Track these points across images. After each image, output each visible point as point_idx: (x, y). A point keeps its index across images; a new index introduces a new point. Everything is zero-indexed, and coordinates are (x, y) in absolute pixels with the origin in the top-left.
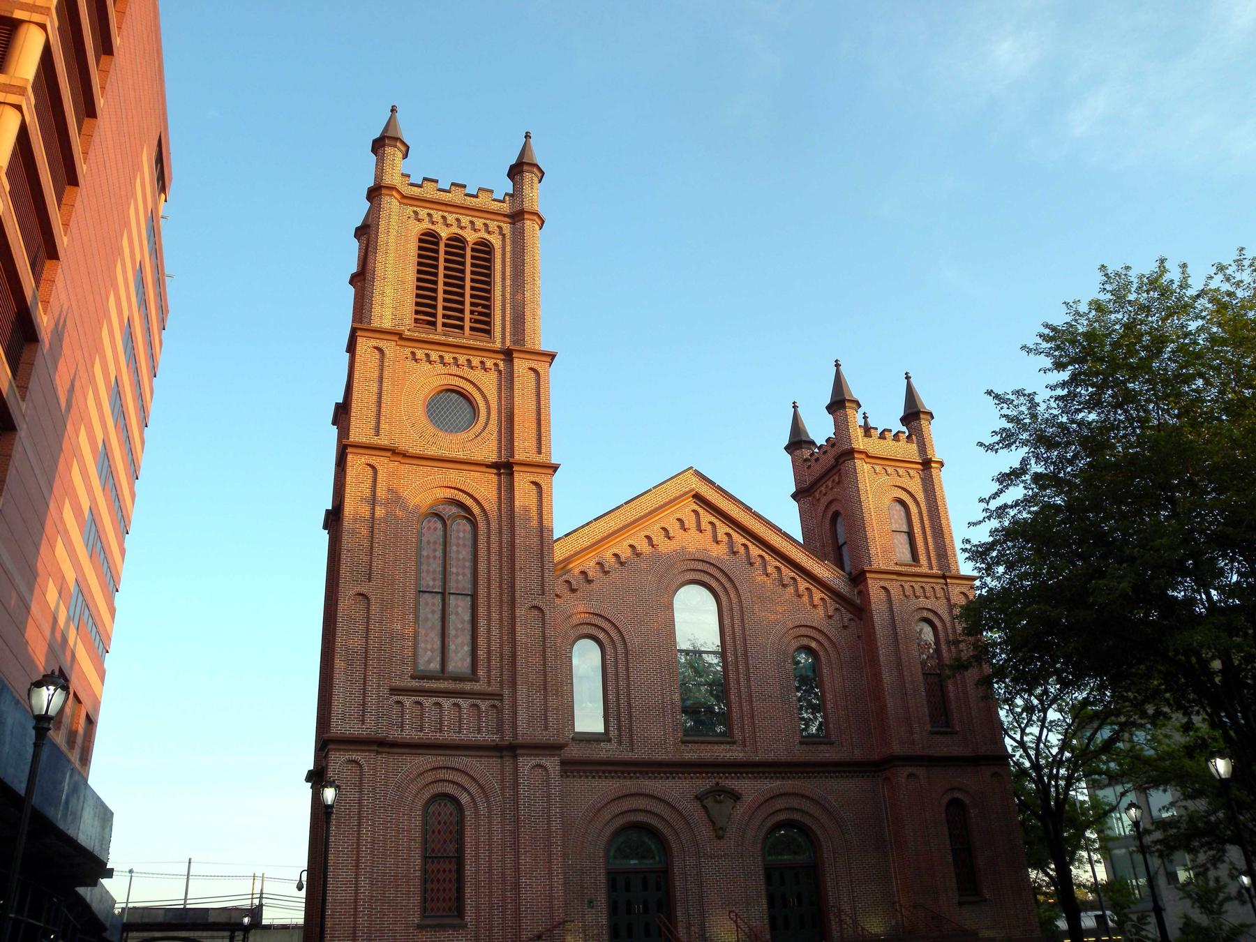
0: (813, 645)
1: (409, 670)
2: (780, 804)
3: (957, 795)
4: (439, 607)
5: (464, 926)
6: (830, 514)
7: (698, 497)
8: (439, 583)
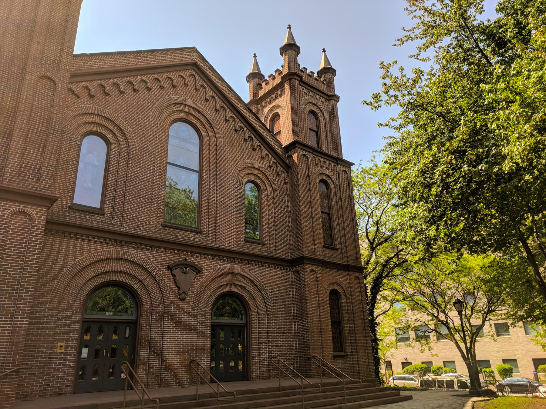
0: (258, 181)
3: (337, 288)
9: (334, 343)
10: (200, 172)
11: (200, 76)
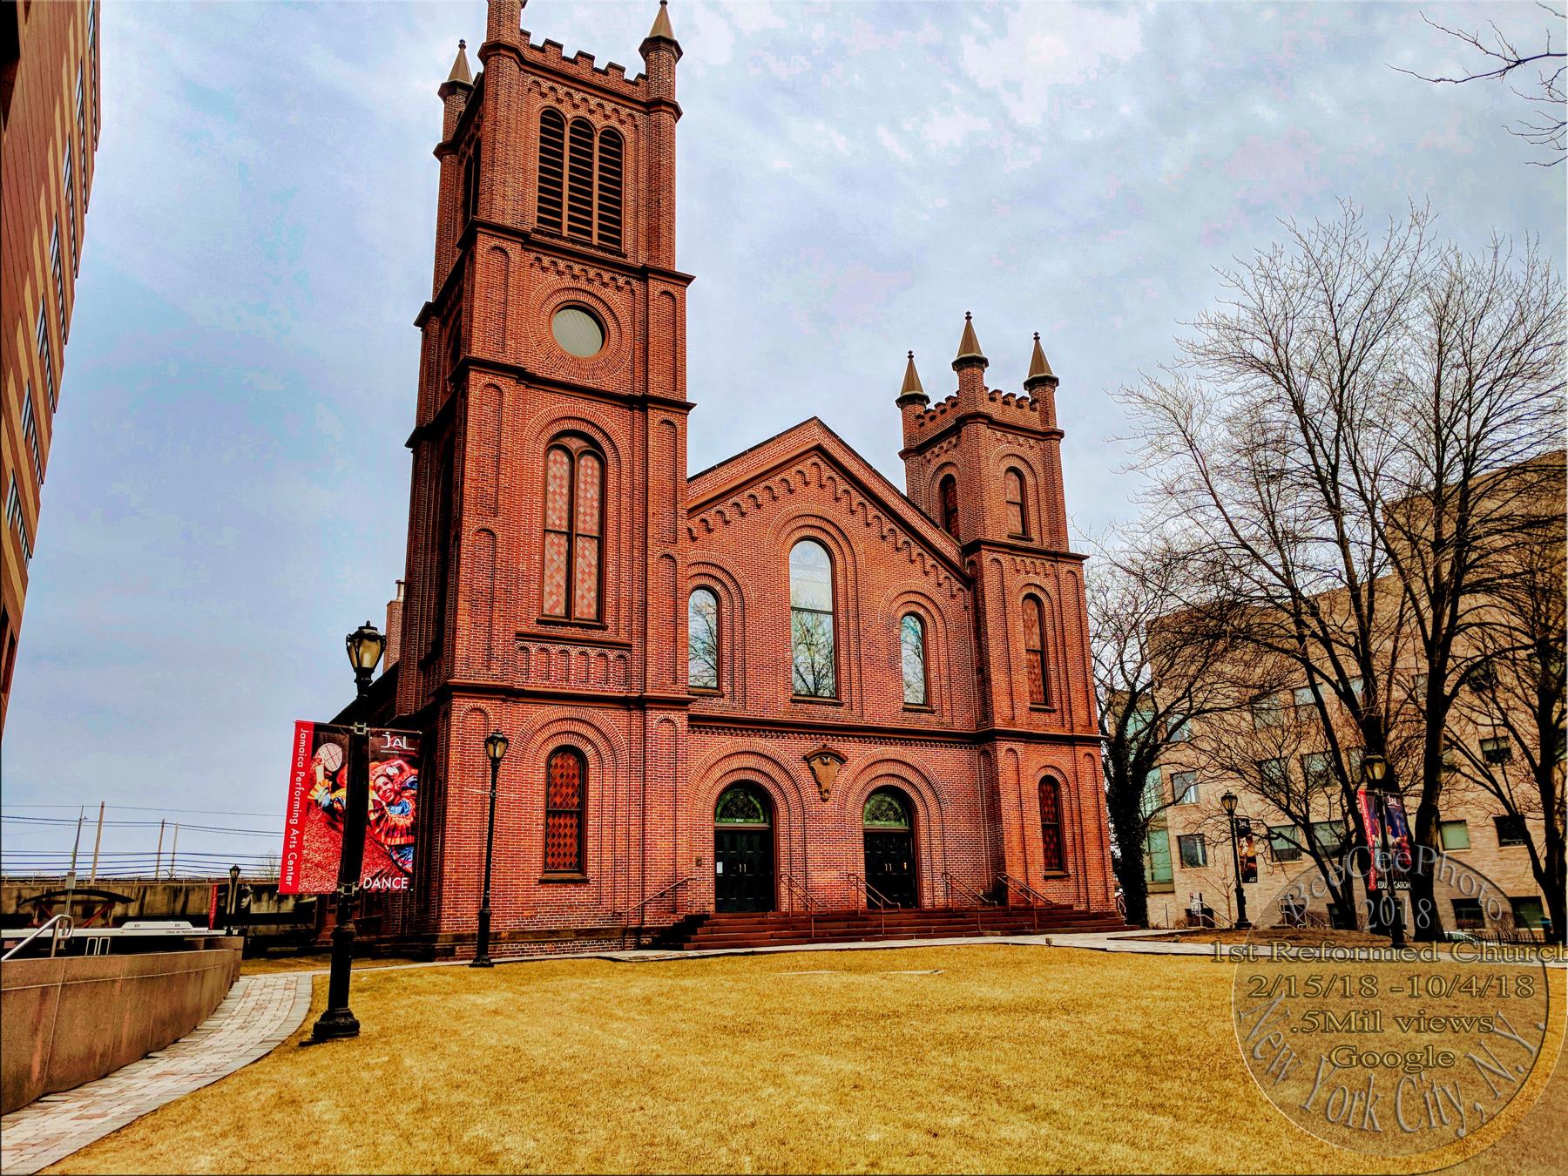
0: (921, 612)
1: (535, 616)
2: (736, 763)
4: (564, 549)
5: (586, 882)
7: (819, 449)
8: (565, 523)
9: (1046, 857)
10: (834, 613)
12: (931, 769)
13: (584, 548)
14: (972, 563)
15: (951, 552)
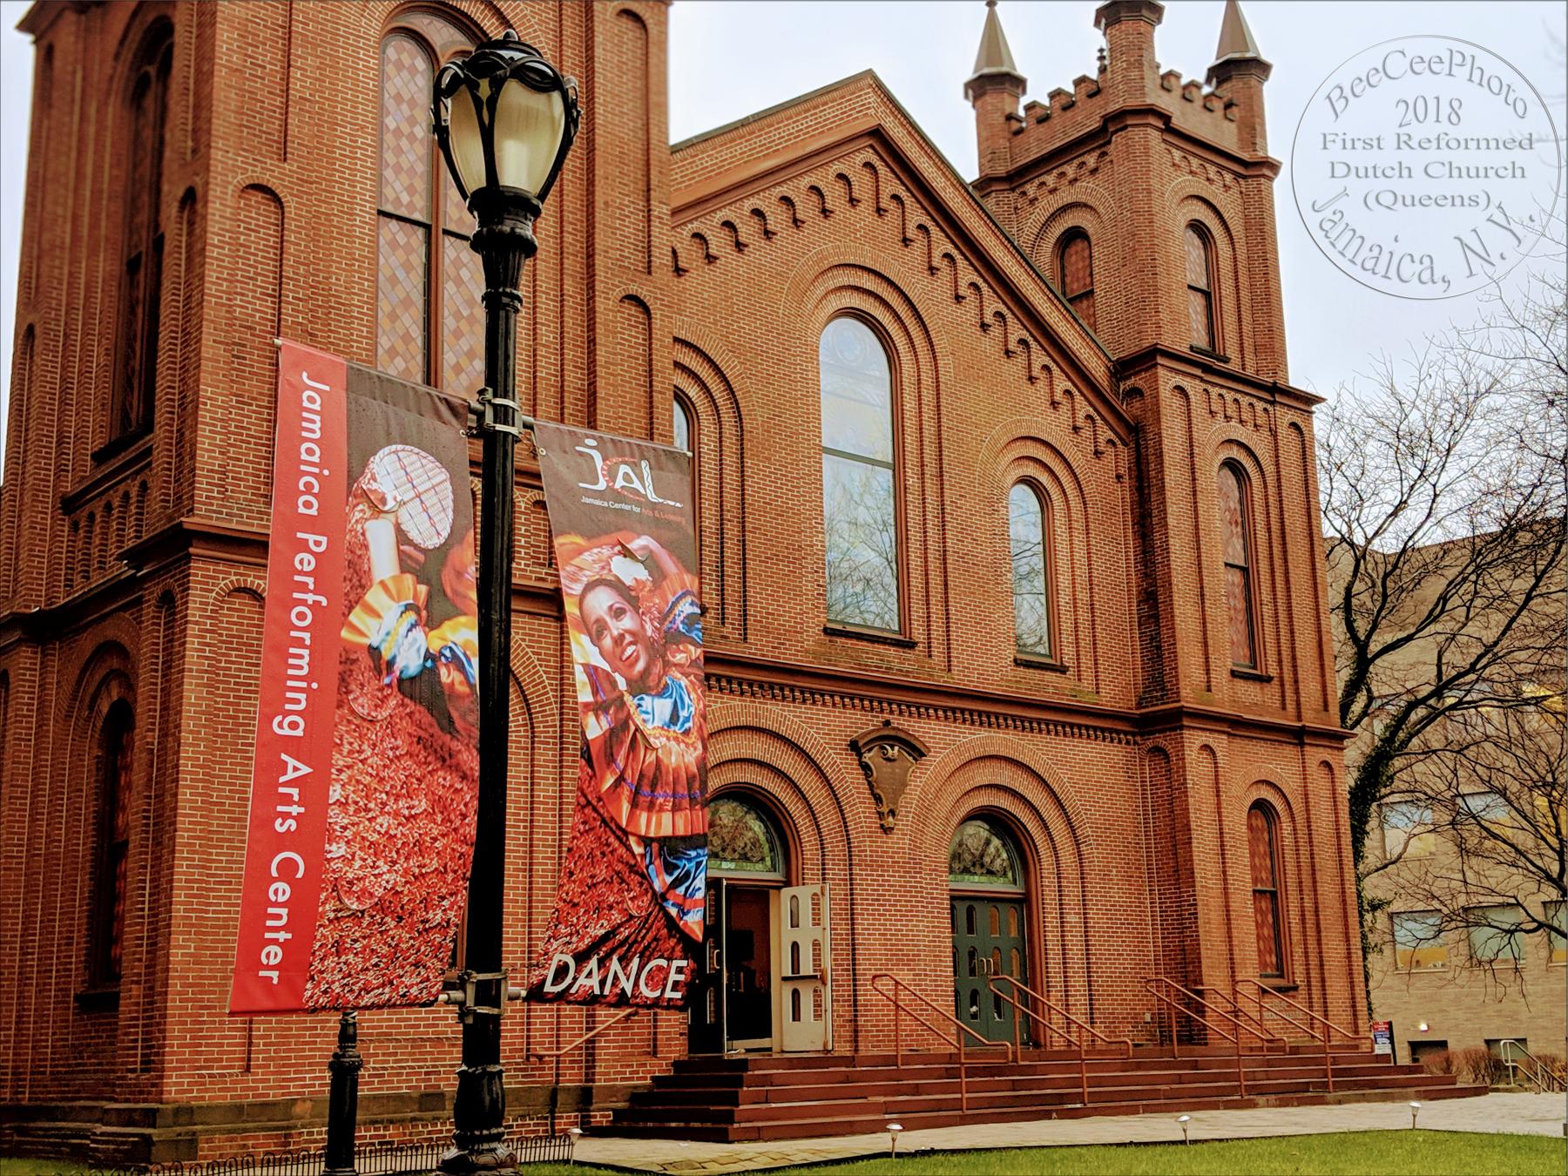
0: (1044, 478)
3: (1267, 794)
4: (418, 259)
6: (1058, 230)
11: (888, 166)
12: (1061, 779)
13: (458, 263)
14: (1135, 392)
15: (1098, 369)
